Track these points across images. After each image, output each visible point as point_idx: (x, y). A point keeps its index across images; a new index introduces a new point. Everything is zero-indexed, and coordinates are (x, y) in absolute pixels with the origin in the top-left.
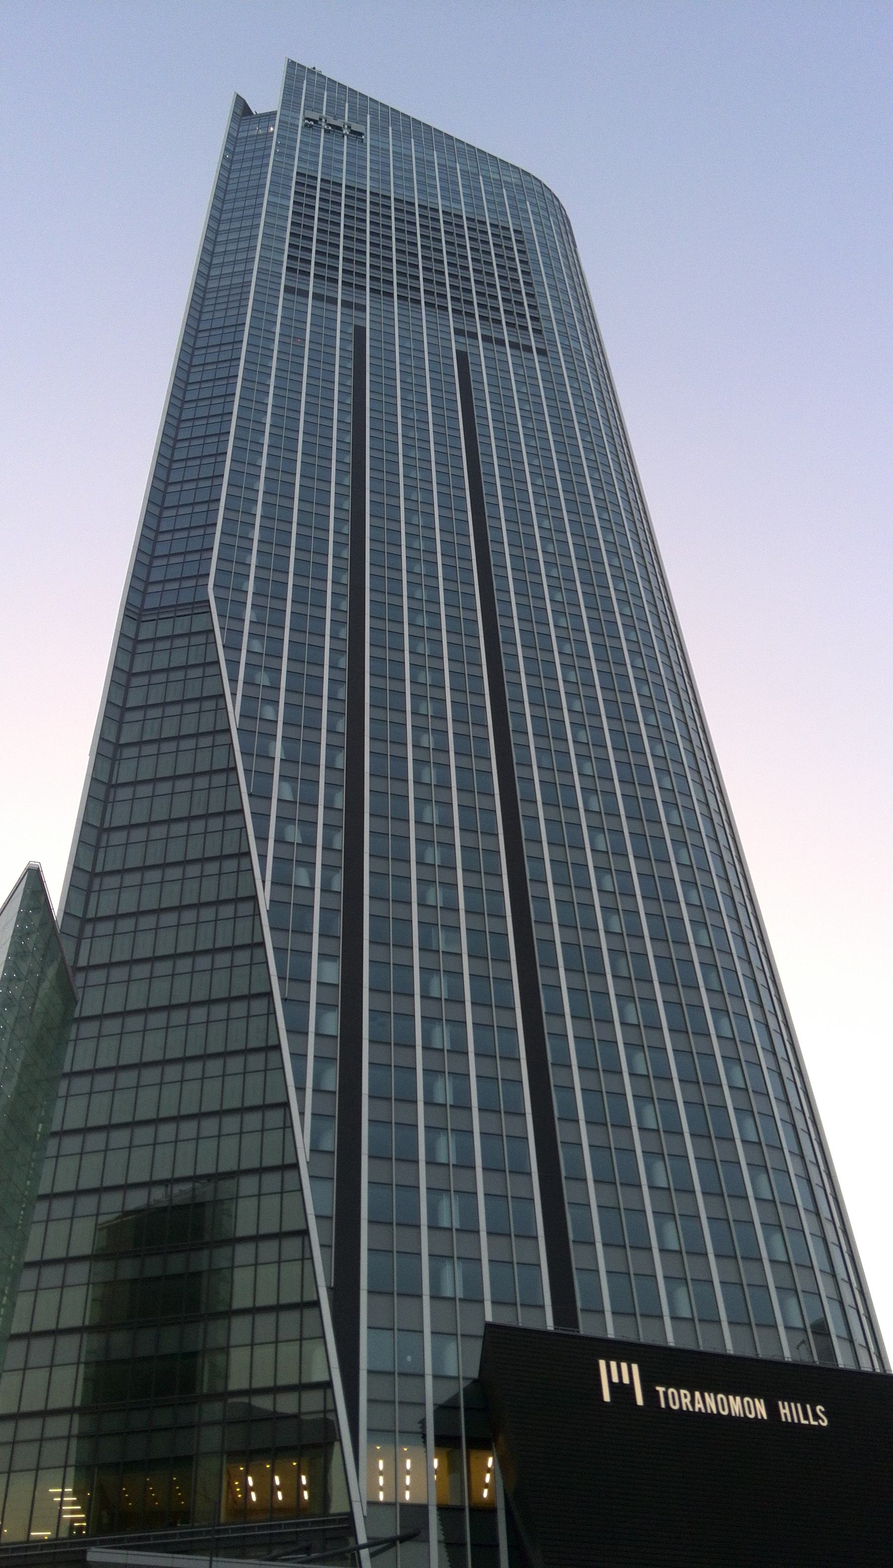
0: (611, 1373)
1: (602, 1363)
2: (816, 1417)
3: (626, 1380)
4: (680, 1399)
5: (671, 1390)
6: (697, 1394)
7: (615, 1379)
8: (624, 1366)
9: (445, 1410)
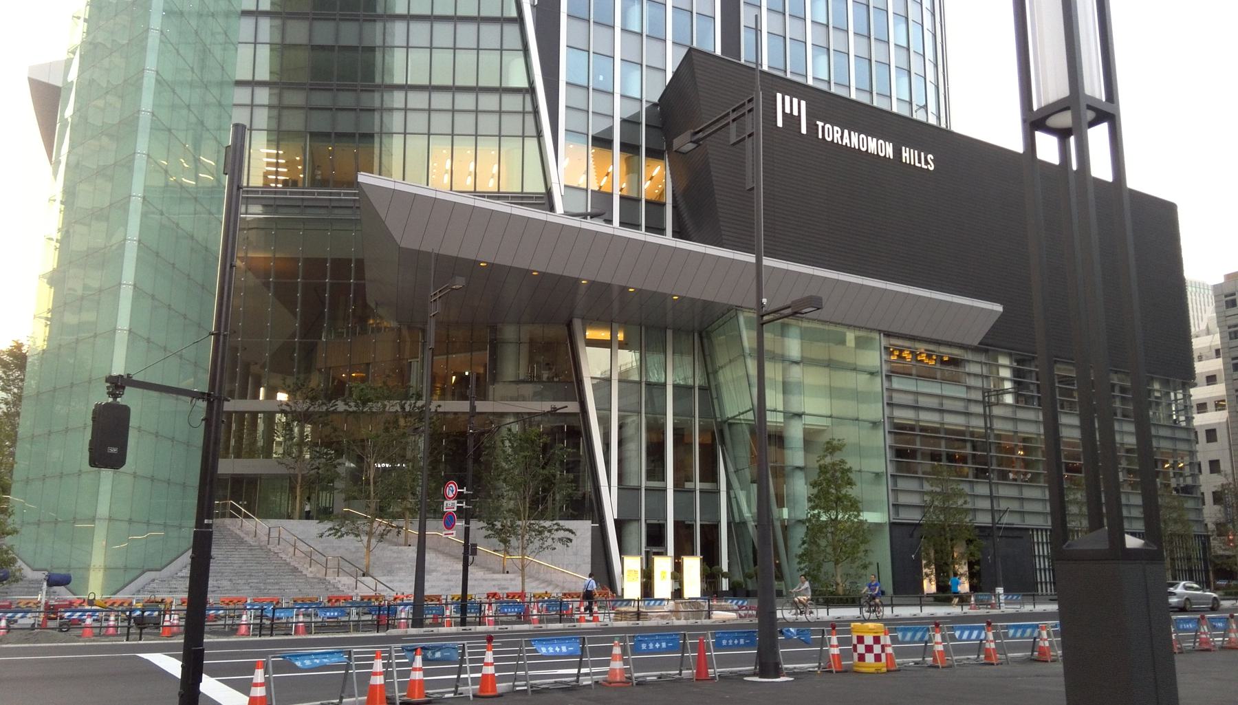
0: (785, 105)
1: (779, 96)
2: (927, 163)
3: (795, 113)
4: (832, 133)
5: (828, 126)
6: (846, 132)
7: (788, 110)
8: (795, 101)
9: (630, 123)
